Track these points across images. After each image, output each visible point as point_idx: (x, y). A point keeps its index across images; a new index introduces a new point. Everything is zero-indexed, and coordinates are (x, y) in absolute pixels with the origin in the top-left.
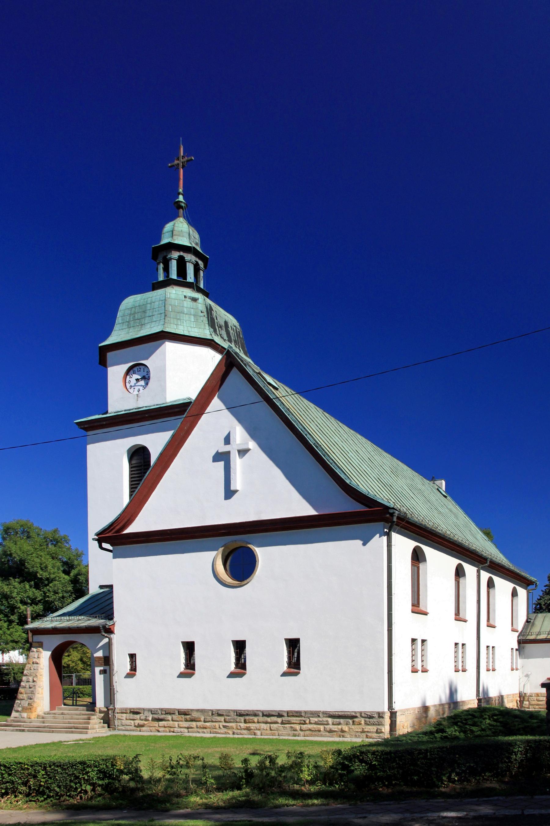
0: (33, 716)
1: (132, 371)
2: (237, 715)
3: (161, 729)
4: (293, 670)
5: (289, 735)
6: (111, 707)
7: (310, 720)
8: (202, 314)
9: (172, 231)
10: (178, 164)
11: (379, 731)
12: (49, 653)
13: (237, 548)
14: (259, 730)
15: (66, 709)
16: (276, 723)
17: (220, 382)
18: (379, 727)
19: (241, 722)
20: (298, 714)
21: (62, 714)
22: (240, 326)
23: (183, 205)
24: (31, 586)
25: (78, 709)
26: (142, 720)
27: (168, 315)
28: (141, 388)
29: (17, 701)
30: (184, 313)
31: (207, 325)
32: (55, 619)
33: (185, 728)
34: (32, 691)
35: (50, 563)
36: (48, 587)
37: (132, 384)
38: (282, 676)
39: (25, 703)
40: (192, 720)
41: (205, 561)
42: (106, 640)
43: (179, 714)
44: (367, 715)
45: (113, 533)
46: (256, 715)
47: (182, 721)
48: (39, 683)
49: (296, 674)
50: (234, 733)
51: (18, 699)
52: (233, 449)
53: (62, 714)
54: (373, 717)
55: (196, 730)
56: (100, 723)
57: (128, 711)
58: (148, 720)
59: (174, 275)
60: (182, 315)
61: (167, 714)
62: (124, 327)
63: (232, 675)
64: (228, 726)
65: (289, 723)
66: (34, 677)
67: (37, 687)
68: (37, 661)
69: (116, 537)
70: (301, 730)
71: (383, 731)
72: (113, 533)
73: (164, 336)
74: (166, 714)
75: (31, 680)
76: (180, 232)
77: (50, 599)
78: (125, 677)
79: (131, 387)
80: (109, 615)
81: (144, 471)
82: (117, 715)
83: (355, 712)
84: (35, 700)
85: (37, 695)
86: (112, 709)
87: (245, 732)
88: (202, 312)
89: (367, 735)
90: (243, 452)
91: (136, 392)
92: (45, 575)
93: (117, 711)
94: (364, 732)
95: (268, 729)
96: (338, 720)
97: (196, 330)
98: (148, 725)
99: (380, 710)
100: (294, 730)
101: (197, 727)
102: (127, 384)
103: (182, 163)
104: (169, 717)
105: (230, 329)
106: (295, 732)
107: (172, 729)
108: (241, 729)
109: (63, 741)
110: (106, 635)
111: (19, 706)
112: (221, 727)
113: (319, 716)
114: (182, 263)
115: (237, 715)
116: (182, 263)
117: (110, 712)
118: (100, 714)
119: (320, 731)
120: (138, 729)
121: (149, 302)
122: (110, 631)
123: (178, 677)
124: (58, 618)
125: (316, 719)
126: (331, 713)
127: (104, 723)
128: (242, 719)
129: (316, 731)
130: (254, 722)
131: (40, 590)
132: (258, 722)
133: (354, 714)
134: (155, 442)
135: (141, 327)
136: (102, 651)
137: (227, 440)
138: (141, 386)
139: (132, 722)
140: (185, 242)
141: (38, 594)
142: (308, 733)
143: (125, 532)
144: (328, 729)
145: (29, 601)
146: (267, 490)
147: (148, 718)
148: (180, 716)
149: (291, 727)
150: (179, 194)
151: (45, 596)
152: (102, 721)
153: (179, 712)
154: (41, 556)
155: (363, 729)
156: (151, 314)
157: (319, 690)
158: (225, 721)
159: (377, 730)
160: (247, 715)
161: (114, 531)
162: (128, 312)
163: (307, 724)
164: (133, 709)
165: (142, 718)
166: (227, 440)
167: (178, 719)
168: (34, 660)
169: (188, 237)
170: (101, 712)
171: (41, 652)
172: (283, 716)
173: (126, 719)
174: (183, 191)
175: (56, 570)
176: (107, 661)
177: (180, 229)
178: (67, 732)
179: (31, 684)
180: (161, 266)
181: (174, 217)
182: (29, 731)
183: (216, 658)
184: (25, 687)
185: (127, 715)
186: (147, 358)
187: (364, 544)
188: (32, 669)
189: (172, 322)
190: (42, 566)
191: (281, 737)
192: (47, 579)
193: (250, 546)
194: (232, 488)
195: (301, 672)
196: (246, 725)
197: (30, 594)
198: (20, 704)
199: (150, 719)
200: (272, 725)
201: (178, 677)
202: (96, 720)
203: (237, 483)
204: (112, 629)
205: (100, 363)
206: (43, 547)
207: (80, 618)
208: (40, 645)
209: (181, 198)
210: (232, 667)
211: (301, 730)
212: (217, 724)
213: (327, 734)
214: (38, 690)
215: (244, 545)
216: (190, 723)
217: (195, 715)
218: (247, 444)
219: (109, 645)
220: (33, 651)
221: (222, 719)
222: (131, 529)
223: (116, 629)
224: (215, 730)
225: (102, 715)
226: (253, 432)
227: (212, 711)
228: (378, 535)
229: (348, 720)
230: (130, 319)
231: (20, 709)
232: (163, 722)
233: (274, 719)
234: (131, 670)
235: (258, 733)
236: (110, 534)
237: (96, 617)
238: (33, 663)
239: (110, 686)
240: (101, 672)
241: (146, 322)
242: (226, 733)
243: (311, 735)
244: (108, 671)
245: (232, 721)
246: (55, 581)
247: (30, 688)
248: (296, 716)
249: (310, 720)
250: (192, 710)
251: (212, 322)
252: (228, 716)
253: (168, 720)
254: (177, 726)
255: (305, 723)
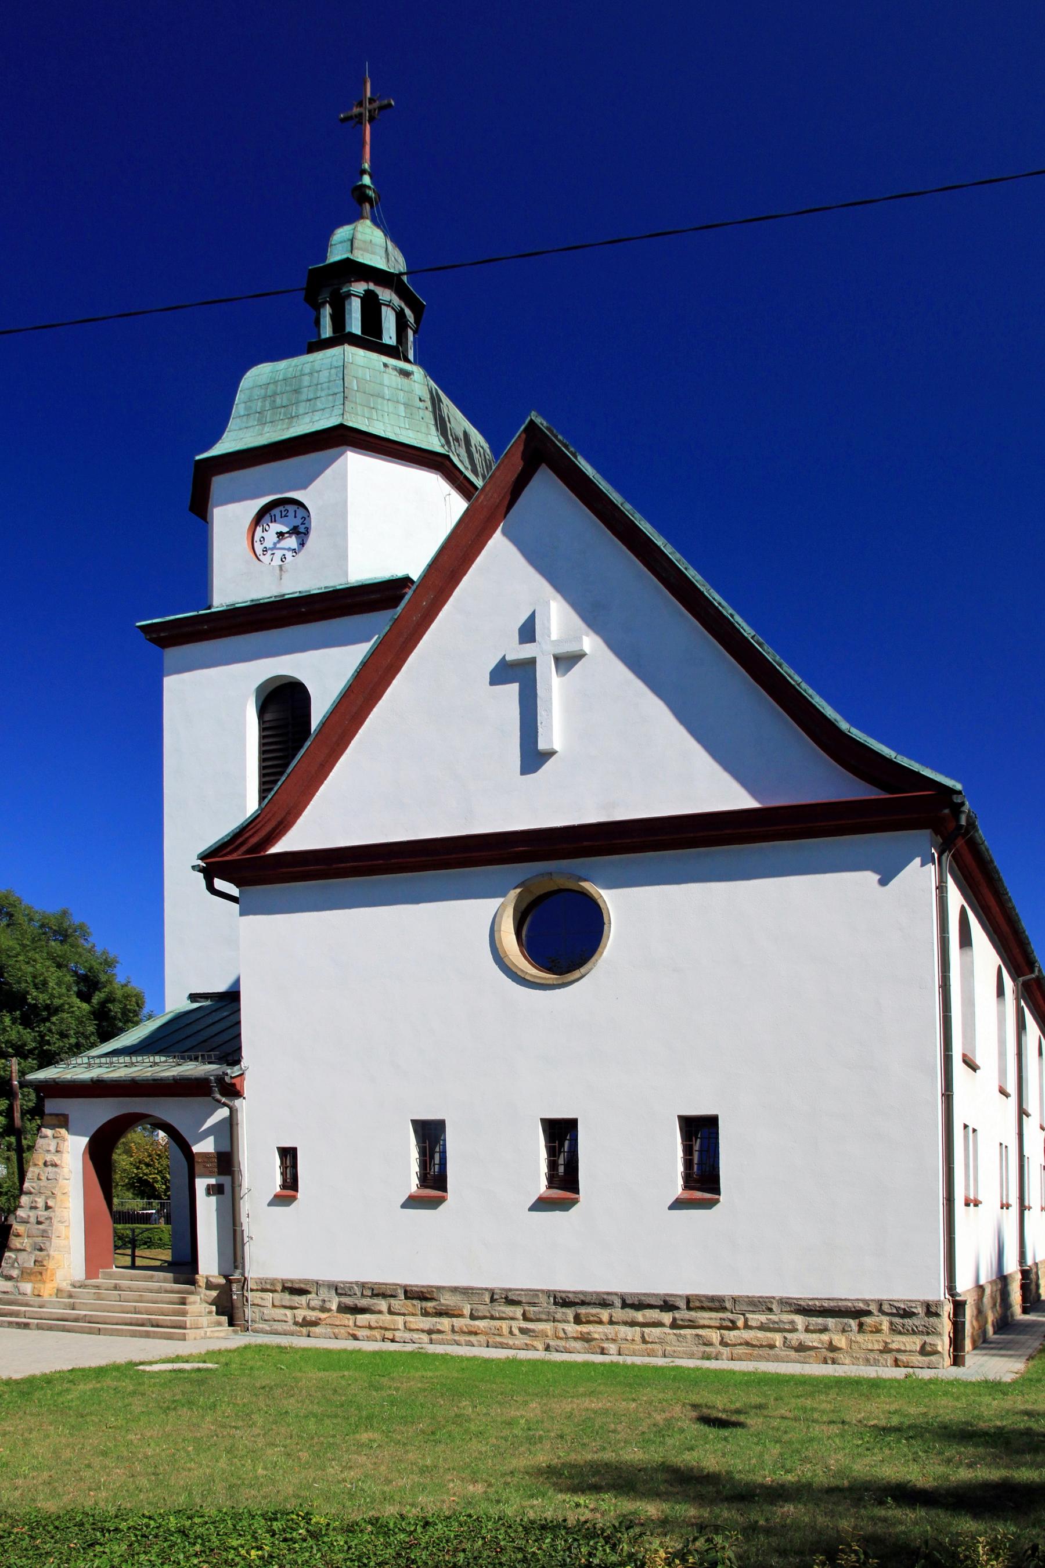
0: (48, 1290)
1: (267, 517)
2: (555, 1303)
3: (360, 1333)
4: (699, 1195)
5: (691, 1356)
6: (237, 1276)
7: (746, 1320)
8: (421, 405)
9: (352, 241)
10: (361, 115)
11: (928, 1349)
12: (85, 1141)
13: (554, 895)
14: (614, 1340)
15: (123, 1277)
16: (659, 1324)
17: (508, 498)
18: (928, 1339)
19: (568, 1322)
20: (715, 1304)
21: (116, 1288)
22: (491, 448)
23: (371, 193)
24: (14, 1021)
25: (152, 1277)
26: (313, 1309)
27: (350, 398)
28: (289, 554)
29: (7, 1254)
30: (383, 398)
31: (433, 428)
32: (97, 1061)
33: (423, 1331)
34: (44, 1231)
35: (53, 976)
36: (48, 1024)
37: (268, 544)
38: (671, 1208)
39: (27, 1260)
40: (440, 1314)
41: (476, 921)
42: (223, 1113)
43: (406, 1298)
44: (898, 1308)
45: (243, 854)
46: (604, 1304)
47: (413, 1315)
48: (58, 1213)
49: (710, 1204)
50: (547, 1348)
51: (11, 1250)
52: (542, 652)
53: (116, 1288)
54: (914, 1314)
55: (450, 1336)
56: (210, 1312)
57: (279, 1288)
58: (329, 1310)
59: (355, 326)
60: (380, 400)
61: (377, 1295)
62: (250, 424)
63: (542, 1204)
64: (533, 1331)
65: (692, 1325)
66: (47, 1198)
67: (55, 1221)
68: (56, 1159)
69: (247, 865)
70: (724, 1343)
71: (939, 1349)
72: (243, 854)
73: (343, 437)
74: (374, 1295)
75: (41, 1204)
76: (368, 243)
77: (53, 1048)
78: (269, 1205)
79: (265, 550)
80: (229, 1054)
81: (294, 740)
82: (250, 1295)
83: (866, 1302)
84: (52, 1253)
85: (55, 1241)
86: (238, 1281)
87: (578, 1345)
88: (420, 400)
89: (896, 1360)
90: (566, 661)
91: (277, 562)
92: (43, 998)
93: (251, 1285)
94: (890, 1351)
95: (638, 1338)
96: (820, 1320)
97: (411, 434)
98: (328, 1321)
99: (930, 1297)
100: (705, 1344)
101: (453, 1331)
102: (257, 545)
103: (370, 111)
104: (383, 1304)
105: (473, 449)
106: (708, 1349)
107: (389, 1335)
108: (567, 1338)
109: (137, 1359)
110: (223, 1100)
111: (13, 1266)
112: (516, 1331)
113: (770, 1310)
114: (371, 307)
115: (555, 1303)
116: (371, 307)
117: (234, 1287)
118: (208, 1292)
119: (772, 1347)
120: (304, 1330)
121: (307, 371)
122: (232, 1091)
123: (404, 1206)
124: (103, 1060)
125: (763, 1318)
126: (802, 1303)
127: (218, 1313)
128: (570, 1313)
129: (762, 1346)
130: (600, 1322)
131: (33, 1029)
132: (611, 1322)
133: (861, 1305)
134: (325, 670)
135: (291, 423)
136: (211, 1139)
137: (528, 632)
138: (289, 549)
139: (288, 1312)
140: (378, 262)
141: (29, 1037)
142: (741, 1350)
143: (274, 850)
144: (795, 1343)
145: (10, 1050)
146: (629, 747)
147: (327, 1305)
148: (409, 1302)
149: (697, 1335)
150: (363, 172)
151: (42, 1040)
152: (214, 1308)
153: (406, 1292)
154: (34, 961)
155: (886, 1343)
156: (311, 396)
157: (753, 1247)
158: (525, 1318)
159: (923, 1346)
160: (583, 1303)
161: (244, 848)
162: (258, 392)
163: (738, 1328)
164: (292, 1281)
165: (313, 1303)
166: (528, 632)
167: (403, 1311)
168: (49, 1158)
169: (383, 254)
170: (210, 1286)
171: (64, 1140)
172: (677, 1308)
173: (274, 1306)
174: (371, 167)
175: (64, 991)
176: (226, 1163)
177: (368, 238)
178: (134, 1334)
179: (42, 1214)
180: (327, 311)
181: (353, 218)
182: (39, 1327)
183: (496, 1163)
184: (25, 1222)
185: (276, 1295)
186: (304, 486)
187: (883, 882)
188: (43, 1178)
189: (359, 413)
190: (37, 981)
191: (629, 1360)
192: (47, 1007)
193: (587, 885)
194: (542, 746)
195: (721, 1198)
196: (579, 1328)
197: (13, 1036)
198: (16, 1260)
199: (334, 1307)
200: (646, 1330)
201: (404, 1206)
202: (199, 1306)
203: (554, 733)
204: (238, 1087)
205: (192, 509)
206: (39, 944)
207: (157, 1059)
208: (62, 1121)
209: (367, 180)
210: (541, 1186)
211: (724, 1343)
212: (504, 1325)
213: (793, 1354)
214: (58, 1228)
215: (570, 885)
216: (435, 1319)
217: (447, 1300)
218: (580, 640)
219: (230, 1125)
220: (46, 1137)
221: (518, 1311)
222: (287, 844)
223: (248, 1087)
224: (498, 1339)
225: (214, 1293)
226: (592, 613)
227: (492, 1292)
228: (917, 861)
229: (845, 1320)
230: (264, 406)
231: (15, 1273)
232: (367, 1316)
233: (654, 1315)
234: (284, 1186)
235: (612, 1348)
236: (234, 856)
237: (196, 1059)
238: (45, 1164)
239: (234, 1224)
240: (210, 1190)
241: (301, 411)
242: (527, 1347)
243: (749, 1358)
244: (227, 1189)
245: (544, 1317)
246: (63, 1011)
247: (39, 1223)
248: (711, 1309)
249: (746, 1320)
250: (439, 1288)
251: (442, 425)
252: (534, 1304)
253: (380, 1312)
254: (401, 1326)
255: (734, 1327)
